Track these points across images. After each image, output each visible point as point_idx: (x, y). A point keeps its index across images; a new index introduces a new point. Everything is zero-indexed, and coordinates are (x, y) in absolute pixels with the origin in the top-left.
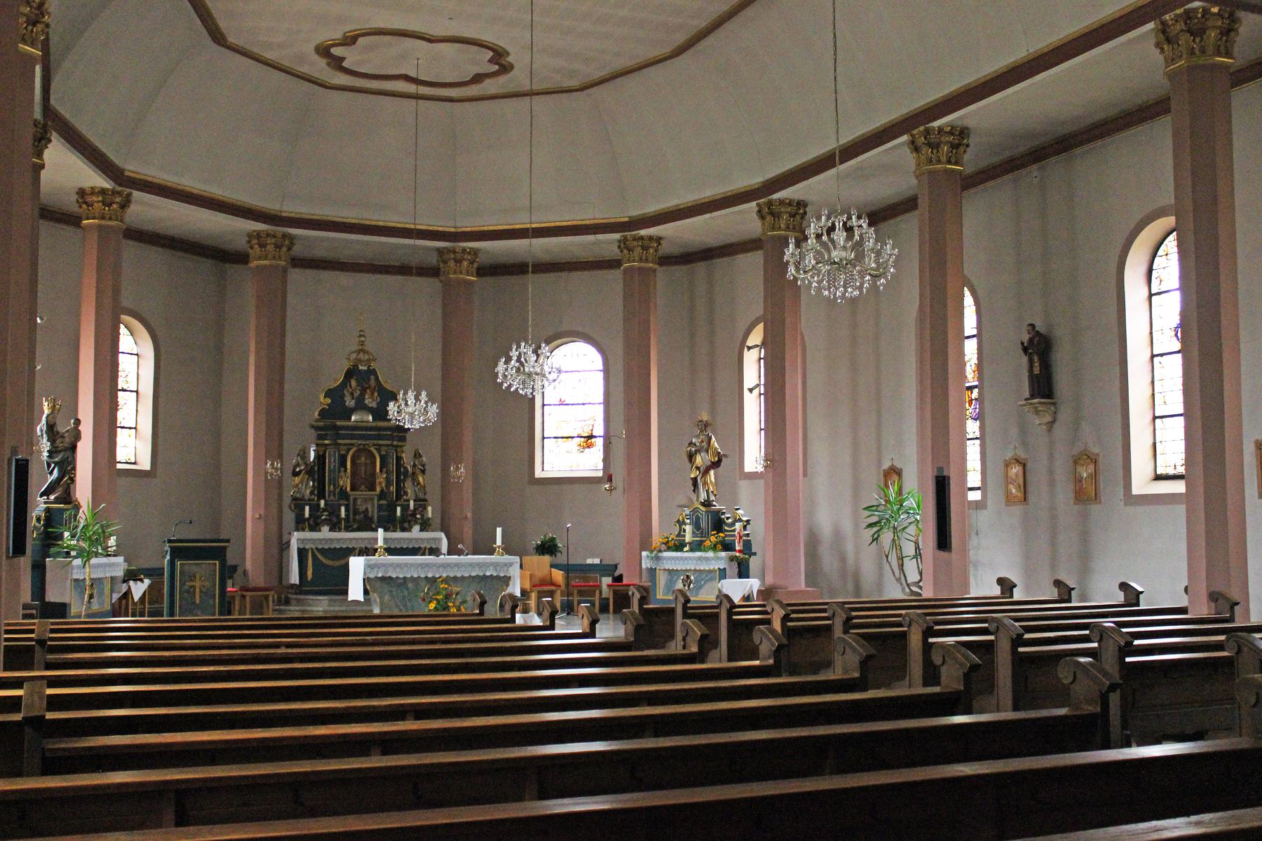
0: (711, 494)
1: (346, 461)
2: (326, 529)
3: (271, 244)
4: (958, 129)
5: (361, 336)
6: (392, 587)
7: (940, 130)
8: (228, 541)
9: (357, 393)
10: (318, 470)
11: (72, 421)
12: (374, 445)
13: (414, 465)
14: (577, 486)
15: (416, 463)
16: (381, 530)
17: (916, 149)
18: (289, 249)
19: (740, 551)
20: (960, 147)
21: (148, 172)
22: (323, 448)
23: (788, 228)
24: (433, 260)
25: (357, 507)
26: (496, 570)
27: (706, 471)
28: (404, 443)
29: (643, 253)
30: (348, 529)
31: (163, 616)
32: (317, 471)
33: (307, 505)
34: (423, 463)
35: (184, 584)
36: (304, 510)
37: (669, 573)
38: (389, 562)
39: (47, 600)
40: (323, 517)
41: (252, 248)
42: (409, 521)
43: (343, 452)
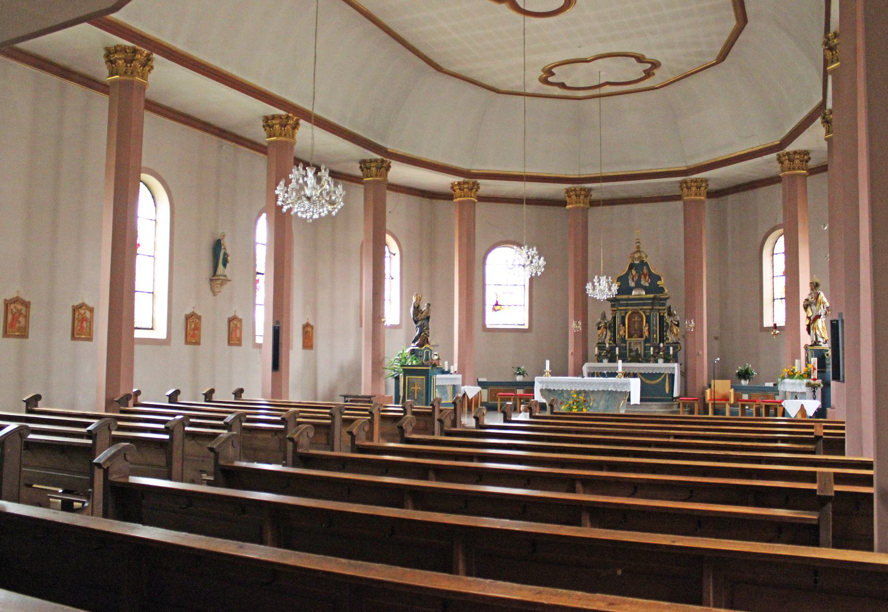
0: (818, 337)
2: (605, 361)
3: (573, 195)
5: (638, 242)
9: (636, 278)
10: (663, 328)
11: (426, 305)
12: (641, 309)
13: (672, 321)
14: (497, 334)
16: (620, 362)
25: (632, 348)
26: (615, 387)
29: (790, 164)
33: (671, 346)
34: (677, 320)
36: (669, 350)
40: (603, 354)
43: (623, 315)
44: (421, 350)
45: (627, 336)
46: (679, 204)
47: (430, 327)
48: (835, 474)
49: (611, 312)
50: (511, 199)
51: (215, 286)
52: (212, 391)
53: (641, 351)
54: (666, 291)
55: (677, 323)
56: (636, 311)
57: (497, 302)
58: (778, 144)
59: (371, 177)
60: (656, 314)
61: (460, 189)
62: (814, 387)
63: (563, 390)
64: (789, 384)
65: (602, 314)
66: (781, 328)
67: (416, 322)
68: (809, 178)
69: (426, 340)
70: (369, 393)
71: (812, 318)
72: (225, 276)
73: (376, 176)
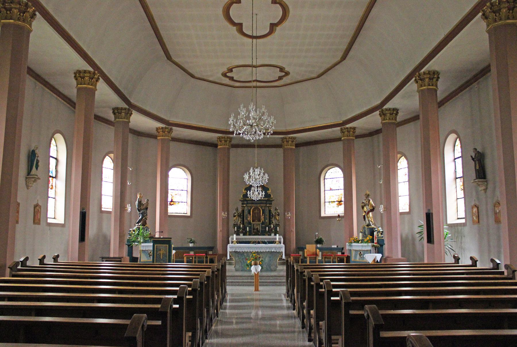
1: (250, 212)
2: (241, 235)
4: (432, 72)
7: (424, 73)
8: (171, 238)
11: (146, 200)
12: (260, 206)
13: (275, 213)
16: (235, 235)
17: (417, 82)
18: (230, 142)
19: (376, 243)
20: (434, 79)
21: (178, 121)
22: (243, 208)
23: (390, 119)
24: (279, 142)
28: (271, 205)
30: (249, 235)
31: (204, 263)
32: (242, 215)
37: (355, 251)
39: (133, 256)
40: (240, 231)
41: (218, 142)
42: (270, 232)
43: (249, 209)
45: (251, 221)
46: (280, 151)
48: (350, 292)
49: (241, 207)
51: (30, 182)
52: (58, 256)
53: (260, 228)
54: (272, 196)
55: (278, 214)
56: (257, 207)
57: (172, 200)
58: (342, 123)
60: (267, 209)
62: (376, 247)
63: (258, 251)
64: (355, 246)
66: (342, 217)
67: (139, 211)
70: (117, 256)
72: (37, 175)
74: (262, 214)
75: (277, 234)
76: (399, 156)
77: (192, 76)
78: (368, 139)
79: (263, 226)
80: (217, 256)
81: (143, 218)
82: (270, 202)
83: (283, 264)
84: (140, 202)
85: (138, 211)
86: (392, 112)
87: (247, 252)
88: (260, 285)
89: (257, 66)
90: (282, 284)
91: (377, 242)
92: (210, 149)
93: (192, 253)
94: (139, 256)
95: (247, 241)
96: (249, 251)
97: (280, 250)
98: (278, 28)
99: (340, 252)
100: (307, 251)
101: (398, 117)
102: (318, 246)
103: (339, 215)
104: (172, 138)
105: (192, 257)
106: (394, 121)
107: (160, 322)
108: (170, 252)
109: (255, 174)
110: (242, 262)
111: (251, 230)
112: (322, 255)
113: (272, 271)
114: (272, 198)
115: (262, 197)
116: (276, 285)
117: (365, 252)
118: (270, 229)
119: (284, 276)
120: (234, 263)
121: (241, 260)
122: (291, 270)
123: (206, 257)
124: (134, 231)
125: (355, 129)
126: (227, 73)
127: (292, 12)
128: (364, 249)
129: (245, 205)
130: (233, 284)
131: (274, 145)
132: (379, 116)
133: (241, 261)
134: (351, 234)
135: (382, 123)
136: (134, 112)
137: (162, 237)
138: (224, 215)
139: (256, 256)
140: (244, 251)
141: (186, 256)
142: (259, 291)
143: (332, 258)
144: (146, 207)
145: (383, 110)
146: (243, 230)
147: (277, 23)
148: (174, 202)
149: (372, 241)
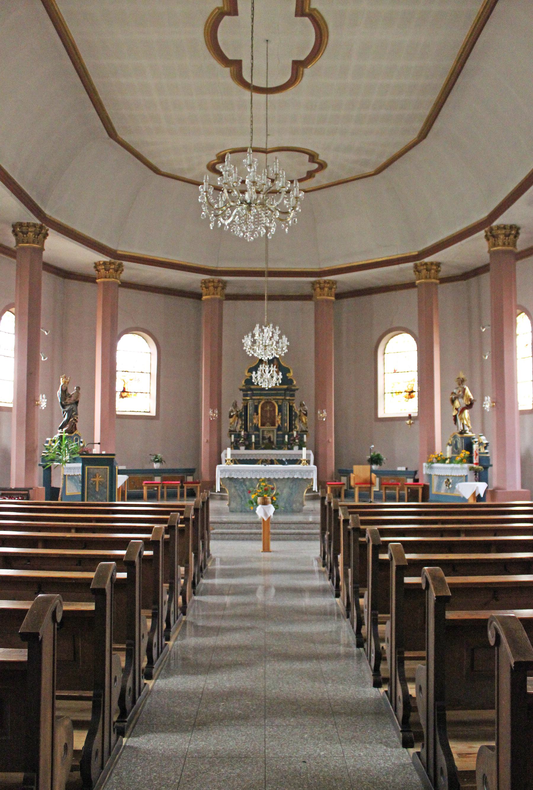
2: (242, 448)
6: (236, 484)
8: (114, 455)
11: (75, 388)
12: (274, 399)
13: (300, 411)
15: (301, 409)
16: (229, 449)
19: (476, 464)
22: (246, 402)
24: (308, 290)
25: (265, 435)
26: (301, 474)
27: (462, 411)
30: (256, 448)
32: (243, 415)
34: (305, 410)
35: (90, 480)
38: (232, 469)
39: (52, 486)
40: (240, 442)
41: (203, 289)
42: (291, 444)
43: (256, 404)
44: (71, 437)
46: (310, 305)
47: (79, 413)
49: (243, 402)
50: (141, 285)
53: (274, 439)
54: (295, 382)
55: (305, 413)
56: (269, 400)
57: (124, 388)
59: (27, 243)
61: (105, 269)
62: (476, 471)
64: (438, 468)
65: (233, 403)
66: (415, 418)
67: (63, 406)
68: (225, 302)
69: (74, 426)
70: (22, 485)
71: (459, 410)
73: (34, 242)
74: (278, 413)
75: (304, 447)
76: (518, 311)
77: (156, 171)
78: (461, 285)
79: (280, 433)
80: (200, 485)
81: (71, 420)
82: (291, 393)
83: (314, 498)
84: (64, 392)
85: (61, 408)
86: (508, 231)
87: (251, 479)
88: (273, 540)
89: (268, 150)
90: (313, 537)
91: (478, 462)
92: (190, 302)
93: (158, 479)
94: (61, 486)
95: (252, 458)
96: (253, 477)
97: (309, 475)
98: (308, 71)
99: (410, 478)
100: (354, 477)
101: (518, 242)
102: (374, 467)
103: (410, 415)
104: (121, 282)
105: (158, 487)
106: (510, 248)
107: (126, 574)
108: (113, 481)
109: (263, 337)
110: (242, 496)
111: (259, 441)
112: (381, 484)
113: (293, 512)
114: (294, 386)
115: (278, 382)
116: (302, 539)
117: (457, 479)
118: (292, 439)
119: (316, 524)
120: (228, 498)
121: (240, 494)
122: (330, 518)
123: (182, 487)
124: (54, 442)
125: (439, 266)
126: (218, 163)
127: (333, 37)
128: (455, 473)
129: (248, 398)
130: (223, 537)
131: (299, 296)
132: (484, 240)
133: (240, 496)
134: (431, 449)
135: (489, 252)
136: (51, 232)
137: (104, 452)
138: (213, 414)
139: (265, 486)
140: (245, 477)
141: (147, 485)
142: (271, 552)
143: (397, 489)
144: (74, 400)
145: (491, 230)
146: (245, 439)
147: (304, 60)
148: (128, 392)
149: (470, 460)
